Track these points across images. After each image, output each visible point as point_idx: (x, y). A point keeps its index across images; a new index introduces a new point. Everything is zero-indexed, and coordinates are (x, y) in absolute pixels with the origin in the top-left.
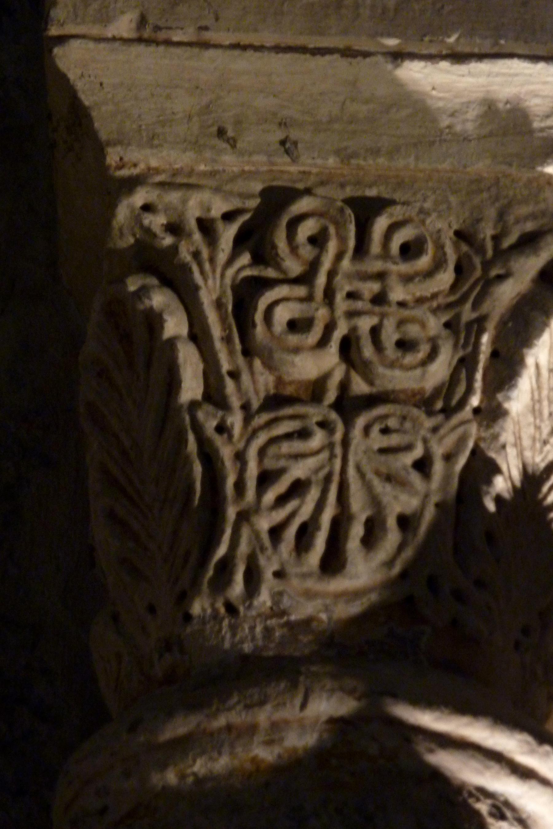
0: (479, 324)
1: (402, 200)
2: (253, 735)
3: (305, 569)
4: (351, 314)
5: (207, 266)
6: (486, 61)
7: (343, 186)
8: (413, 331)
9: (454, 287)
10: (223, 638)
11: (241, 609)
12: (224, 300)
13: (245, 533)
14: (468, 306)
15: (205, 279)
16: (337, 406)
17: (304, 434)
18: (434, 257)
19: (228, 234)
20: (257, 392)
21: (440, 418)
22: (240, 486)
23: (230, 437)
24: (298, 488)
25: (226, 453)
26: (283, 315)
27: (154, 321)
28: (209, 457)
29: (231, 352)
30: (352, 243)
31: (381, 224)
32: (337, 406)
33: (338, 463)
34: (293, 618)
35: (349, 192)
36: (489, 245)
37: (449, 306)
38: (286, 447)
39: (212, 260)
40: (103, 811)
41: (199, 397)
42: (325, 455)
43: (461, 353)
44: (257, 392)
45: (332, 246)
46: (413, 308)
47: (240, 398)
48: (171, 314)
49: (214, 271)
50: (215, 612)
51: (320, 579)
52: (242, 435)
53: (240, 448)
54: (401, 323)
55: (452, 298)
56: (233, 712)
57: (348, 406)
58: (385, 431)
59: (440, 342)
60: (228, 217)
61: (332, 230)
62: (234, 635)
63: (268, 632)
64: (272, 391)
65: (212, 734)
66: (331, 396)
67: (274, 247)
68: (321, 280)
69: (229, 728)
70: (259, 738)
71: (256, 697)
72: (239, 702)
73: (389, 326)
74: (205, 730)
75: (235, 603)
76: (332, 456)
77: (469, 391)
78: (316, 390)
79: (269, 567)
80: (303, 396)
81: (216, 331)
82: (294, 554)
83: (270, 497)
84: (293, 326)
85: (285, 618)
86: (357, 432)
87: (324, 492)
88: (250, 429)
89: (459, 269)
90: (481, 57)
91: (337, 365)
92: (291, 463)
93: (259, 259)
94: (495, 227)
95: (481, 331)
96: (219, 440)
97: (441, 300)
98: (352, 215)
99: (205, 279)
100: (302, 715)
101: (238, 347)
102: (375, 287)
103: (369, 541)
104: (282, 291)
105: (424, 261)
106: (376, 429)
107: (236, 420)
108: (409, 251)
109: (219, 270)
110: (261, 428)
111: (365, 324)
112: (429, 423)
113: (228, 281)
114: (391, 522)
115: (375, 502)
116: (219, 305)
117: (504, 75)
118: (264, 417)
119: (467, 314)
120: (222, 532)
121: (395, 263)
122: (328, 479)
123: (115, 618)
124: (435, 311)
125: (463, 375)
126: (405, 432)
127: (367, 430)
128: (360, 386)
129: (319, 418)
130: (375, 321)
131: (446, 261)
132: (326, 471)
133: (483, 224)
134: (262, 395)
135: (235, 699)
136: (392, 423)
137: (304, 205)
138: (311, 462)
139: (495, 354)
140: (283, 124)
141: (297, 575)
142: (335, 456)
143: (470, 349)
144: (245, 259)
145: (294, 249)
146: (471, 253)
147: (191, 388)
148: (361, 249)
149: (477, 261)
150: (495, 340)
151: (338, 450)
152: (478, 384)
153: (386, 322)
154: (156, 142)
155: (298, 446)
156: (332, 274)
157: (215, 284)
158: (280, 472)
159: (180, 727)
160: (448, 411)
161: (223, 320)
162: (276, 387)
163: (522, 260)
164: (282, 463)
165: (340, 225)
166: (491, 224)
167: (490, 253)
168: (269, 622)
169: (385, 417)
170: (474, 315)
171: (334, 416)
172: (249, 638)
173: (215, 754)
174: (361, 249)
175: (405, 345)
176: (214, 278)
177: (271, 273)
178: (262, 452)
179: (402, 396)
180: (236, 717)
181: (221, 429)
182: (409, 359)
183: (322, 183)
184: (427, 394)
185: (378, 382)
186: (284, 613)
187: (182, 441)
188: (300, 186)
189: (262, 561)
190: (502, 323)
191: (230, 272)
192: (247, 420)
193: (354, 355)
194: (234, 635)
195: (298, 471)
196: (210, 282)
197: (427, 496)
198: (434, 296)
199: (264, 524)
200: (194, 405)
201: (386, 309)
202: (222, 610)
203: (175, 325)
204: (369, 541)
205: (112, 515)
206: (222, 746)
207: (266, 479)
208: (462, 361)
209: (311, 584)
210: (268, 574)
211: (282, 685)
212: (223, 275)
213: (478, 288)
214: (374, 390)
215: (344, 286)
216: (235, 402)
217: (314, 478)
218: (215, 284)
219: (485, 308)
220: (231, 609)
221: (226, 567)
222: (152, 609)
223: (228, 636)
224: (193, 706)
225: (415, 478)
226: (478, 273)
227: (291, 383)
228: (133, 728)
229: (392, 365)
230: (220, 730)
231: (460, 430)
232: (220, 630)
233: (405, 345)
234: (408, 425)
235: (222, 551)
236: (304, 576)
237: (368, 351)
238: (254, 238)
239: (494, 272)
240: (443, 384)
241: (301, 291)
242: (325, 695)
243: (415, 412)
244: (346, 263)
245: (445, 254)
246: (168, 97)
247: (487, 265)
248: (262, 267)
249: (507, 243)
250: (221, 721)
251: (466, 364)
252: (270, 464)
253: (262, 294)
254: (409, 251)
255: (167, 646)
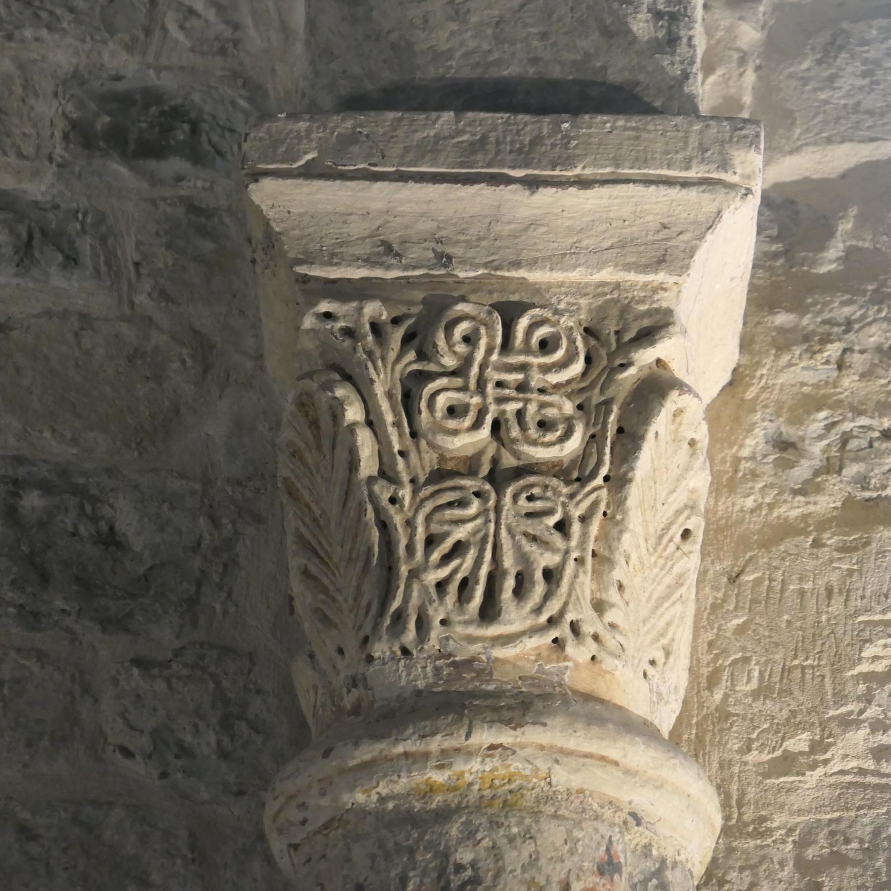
0: (607, 404)
1: (541, 303)
2: (427, 761)
3: (467, 617)
4: (500, 400)
5: (380, 363)
6: (606, 186)
7: (491, 292)
8: (551, 413)
9: (585, 374)
10: (400, 676)
11: (414, 652)
12: (394, 391)
13: (416, 587)
14: (597, 390)
15: (378, 375)
16: (491, 478)
17: (462, 503)
18: (567, 350)
19: (397, 335)
20: (423, 469)
21: (576, 485)
22: (410, 549)
23: (402, 506)
24: (459, 548)
25: (398, 520)
26: (442, 401)
27: (336, 410)
28: (384, 525)
29: (401, 435)
30: (499, 340)
31: (523, 323)
32: (491, 478)
33: (492, 526)
34: (457, 659)
35: (496, 298)
36: (613, 339)
37: (582, 390)
38: (449, 514)
39: (383, 359)
40: (304, 822)
41: (376, 474)
42: (479, 521)
43: (592, 431)
44: (423, 469)
45: (483, 343)
46: (551, 394)
47: (409, 474)
48: (350, 404)
49: (385, 367)
50: (393, 653)
51: (479, 626)
52: (411, 505)
53: (409, 514)
54: (543, 405)
55: (583, 385)
56: (409, 741)
57: (499, 478)
58: (530, 498)
59: (575, 422)
60: (396, 321)
61: (483, 331)
62: (409, 674)
63: (437, 670)
64: (436, 467)
65: (392, 760)
66: (485, 470)
67: (435, 346)
68: (475, 370)
69: (406, 755)
70: (432, 763)
71: (428, 729)
72: (414, 733)
73: (532, 408)
74: (386, 756)
75: (409, 647)
76: (488, 521)
77: (600, 463)
78: (470, 466)
79: (436, 614)
80: (462, 471)
81: (389, 418)
82: (457, 604)
83: (436, 556)
84: (452, 411)
85: (452, 659)
86: (508, 499)
87: (481, 552)
88: (418, 499)
89: (588, 360)
90: (604, 182)
91: (490, 442)
92: (452, 528)
93: (422, 356)
94: (617, 325)
95: (608, 412)
96: (392, 510)
97: (575, 386)
98: (499, 318)
99: (378, 375)
100: (467, 743)
101: (407, 430)
102: (520, 376)
103: (519, 592)
104: (443, 382)
105: (559, 354)
106: (524, 495)
107: (406, 493)
108: (545, 346)
109: (389, 366)
110: (427, 499)
111: (512, 407)
112: (565, 490)
113: (397, 375)
114: (538, 575)
115: (524, 559)
116: (390, 395)
117: (622, 197)
118: (431, 489)
119: (596, 398)
120: (398, 587)
121: (536, 356)
122: (484, 540)
123: (312, 656)
124: (569, 396)
125: (594, 450)
126: (547, 499)
127: (515, 497)
128: (508, 461)
129: (476, 489)
130: (520, 405)
131: (577, 354)
132: (482, 534)
133: (607, 322)
134: (428, 470)
135: (410, 731)
136: (536, 491)
137: (462, 308)
138: (470, 526)
139: (620, 430)
140: (439, 241)
141: (460, 622)
142: (490, 521)
143: (599, 427)
144: (411, 355)
145: (451, 346)
146: (598, 346)
147: (368, 465)
148: (506, 346)
149: (603, 352)
150: (620, 419)
151: (492, 516)
152: (607, 458)
153: (529, 406)
154: (335, 260)
155: (458, 513)
156: (483, 367)
157: (386, 377)
158: (446, 535)
159: (367, 752)
160: (582, 481)
161: (393, 408)
162: (439, 463)
163: (641, 351)
164: (446, 528)
165: (489, 327)
166: (614, 322)
167: (614, 346)
168: (438, 663)
169: (532, 486)
170: (603, 398)
171: (488, 487)
172: (422, 676)
173: (395, 778)
174: (506, 346)
175: (544, 425)
176: (386, 373)
177: (432, 367)
178: (428, 519)
179: (544, 468)
180: (411, 745)
181: (393, 500)
182: (550, 437)
183: (474, 291)
184: (565, 466)
185: (523, 457)
186: (450, 655)
187: (362, 511)
188: (456, 294)
189: (431, 612)
190: (625, 406)
191: (399, 367)
192: (415, 492)
193: (503, 433)
194: (409, 674)
195: (460, 533)
196: (382, 376)
197: (567, 552)
198: (569, 382)
199: (433, 577)
200: (371, 480)
201: (529, 395)
202: (399, 653)
203: (354, 413)
204: (519, 592)
205: (306, 573)
206: (400, 771)
207: (431, 542)
208: (593, 436)
209: (472, 630)
210: (436, 623)
211: (450, 718)
212: (393, 370)
213: (605, 376)
214: (521, 463)
215: (494, 376)
216: (405, 477)
217: (472, 540)
218: (386, 377)
219: (609, 393)
220: (405, 652)
221: (399, 617)
222: (341, 651)
223: (404, 674)
224: (377, 737)
225: (557, 539)
226: (605, 363)
227: (451, 459)
228: (326, 754)
229: (534, 443)
230: (399, 756)
231: (593, 496)
232: (398, 670)
233: (544, 425)
234: (549, 494)
235: (396, 604)
236: (467, 623)
237: (515, 432)
238: (417, 340)
239: (618, 362)
240: (578, 456)
241: (458, 382)
242: (486, 726)
243: (555, 482)
244: (494, 357)
245: (577, 348)
246: (345, 222)
247: (611, 356)
248: (425, 363)
249: (627, 337)
250: (400, 749)
251: (594, 439)
252: (435, 528)
253: (426, 386)
254: (545, 346)
255: (353, 682)
